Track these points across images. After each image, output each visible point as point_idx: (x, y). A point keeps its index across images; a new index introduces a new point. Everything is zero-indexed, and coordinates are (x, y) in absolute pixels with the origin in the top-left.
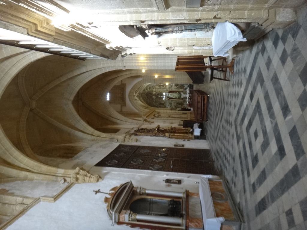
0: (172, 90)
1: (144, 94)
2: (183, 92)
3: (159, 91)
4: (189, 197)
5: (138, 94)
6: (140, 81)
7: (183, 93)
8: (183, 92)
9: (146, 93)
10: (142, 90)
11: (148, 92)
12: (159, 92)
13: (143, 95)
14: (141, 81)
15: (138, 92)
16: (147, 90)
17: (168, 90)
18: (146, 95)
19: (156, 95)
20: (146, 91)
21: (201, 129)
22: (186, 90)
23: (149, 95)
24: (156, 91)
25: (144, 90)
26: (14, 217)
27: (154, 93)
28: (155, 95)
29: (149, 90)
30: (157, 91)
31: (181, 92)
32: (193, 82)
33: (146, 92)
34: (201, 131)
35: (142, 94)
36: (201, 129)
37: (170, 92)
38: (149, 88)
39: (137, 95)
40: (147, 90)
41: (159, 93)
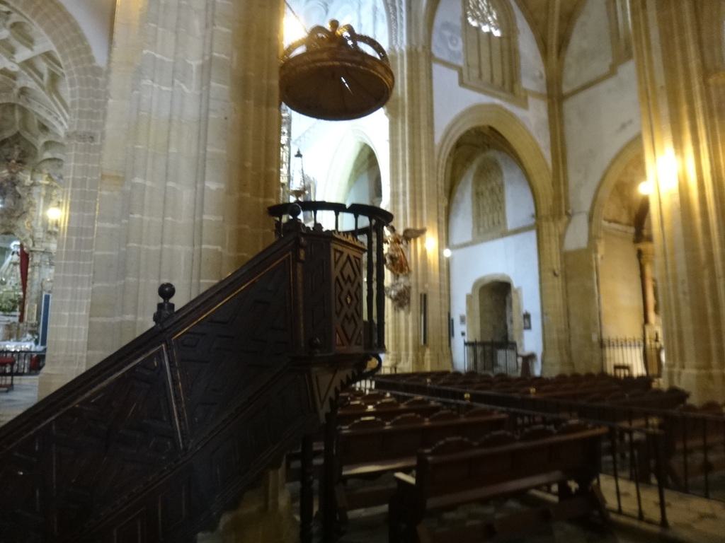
0: (33, 266)
1: (26, 128)
2: (21, 319)
3: (36, 201)
4: (535, 214)
5: (20, 83)
6: (88, 49)
7: (17, 319)
8: (21, 319)
9: (27, 135)
10: (43, 113)
11: (36, 152)
12: (31, 204)
13: (18, 115)
14: (91, 59)
15: (31, 84)
16: (48, 145)
17: (38, 247)
18: (18, 135)
19: (14, 185)
20: (42, 141)
21: (324, 230)
22: (29, 336)
23: (17, 153)
24: (35, 190)
25: (44, 128)
26: (18, 269)
27: (26, 178)
28: (14, 182)
29: (48, 155)
30: (35, 196)
31: (22, 311)
32: (179, 301)
33: (32, 140)
34: (322, 228)
35: (24, 111)
36: (324, 230)
37: (25, 257)
38: (58, 156)
39: (13, 76)
40: (48, 145)
41: (25, 203)
